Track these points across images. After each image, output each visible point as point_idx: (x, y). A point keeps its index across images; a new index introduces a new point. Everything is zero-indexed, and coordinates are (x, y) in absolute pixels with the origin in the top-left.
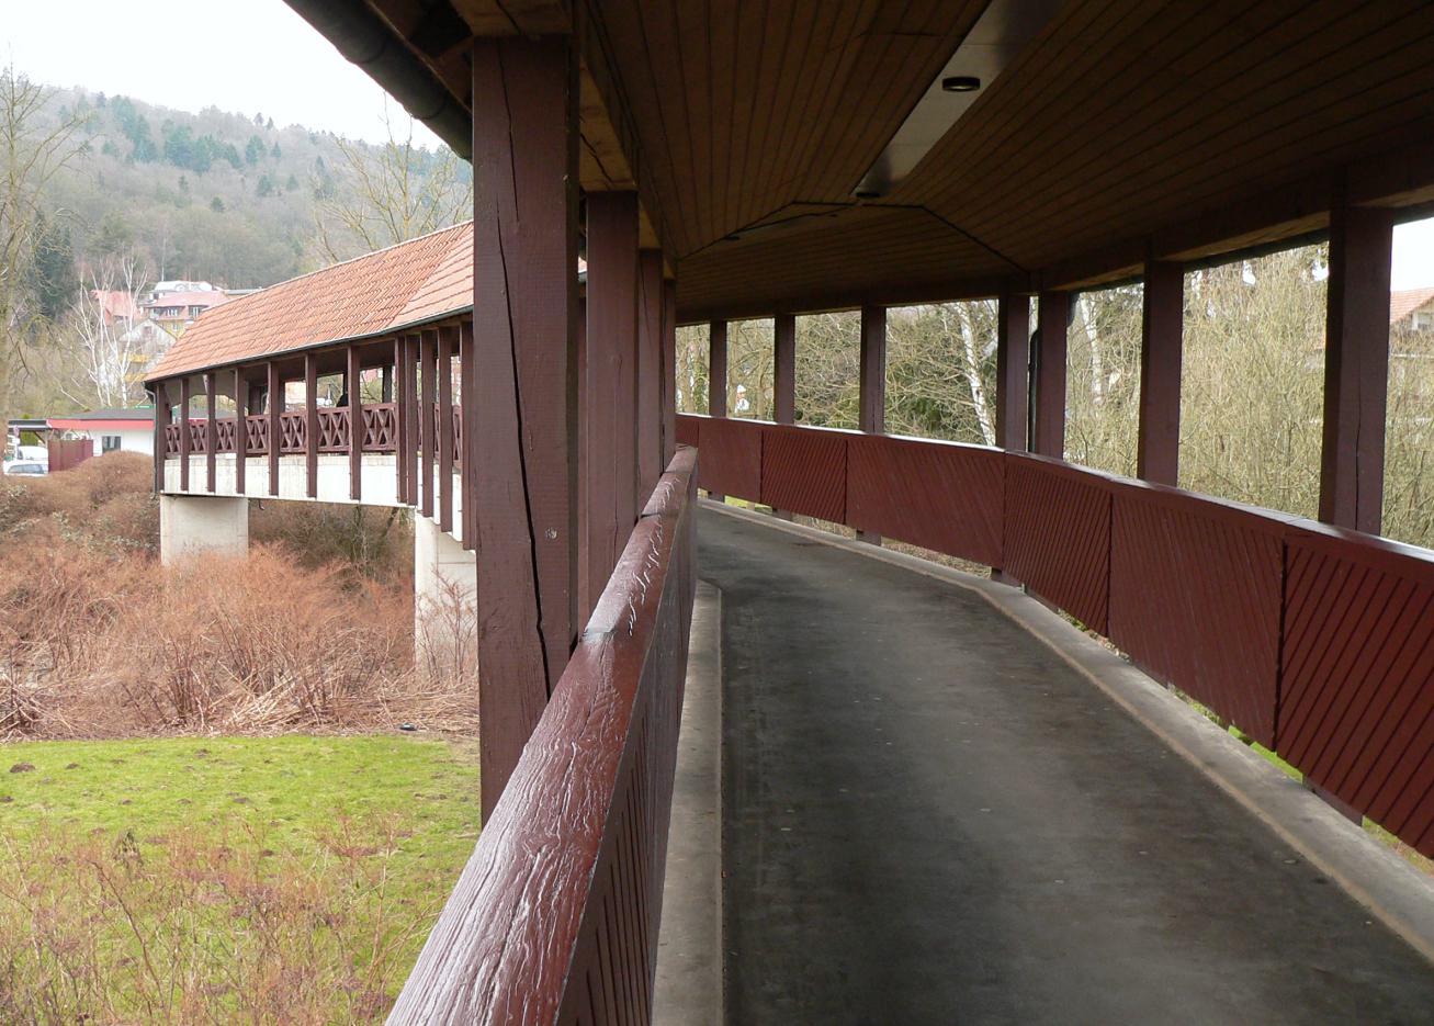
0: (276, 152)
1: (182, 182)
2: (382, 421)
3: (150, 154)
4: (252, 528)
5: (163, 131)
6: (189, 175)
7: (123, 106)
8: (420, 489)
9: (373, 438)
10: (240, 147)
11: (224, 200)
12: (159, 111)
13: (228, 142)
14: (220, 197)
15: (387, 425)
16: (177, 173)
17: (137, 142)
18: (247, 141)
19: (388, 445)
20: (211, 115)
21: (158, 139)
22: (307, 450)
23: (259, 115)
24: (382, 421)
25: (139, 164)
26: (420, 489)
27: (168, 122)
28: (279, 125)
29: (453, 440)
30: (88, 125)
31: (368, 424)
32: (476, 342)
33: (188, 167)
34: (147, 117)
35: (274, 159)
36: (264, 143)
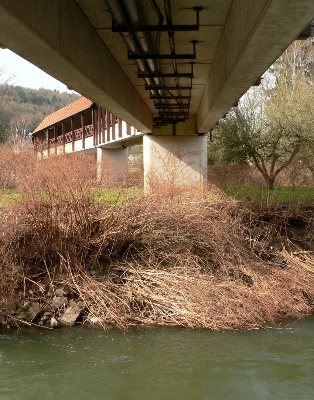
0: (60, 100)
1: (35, 108)
2: (90, 129)
3: (26, 101)
4: (75, 117)
5: (29, 95)
6: (36, 106)
7: (19, 89)
8: (98, 138)
9: (87, 134)
10: (50, 98)
11: (46, 112)
12: (28, 89)
13: (46, 97)
14: (45, 111)
15: (91, 130)
16: (33, 105)
17: (22, 98)
18: (52, 97)
19: (91, 134)
20: (42, 90)
21: (27, 96)
22: (72, 141)
23: (55, 90)
24: (90, 129)
25: (23, 103)
26: (98, 138)
27: (31, 92)
28: (61, 92)
29: (110, 119)
30: (10, 94)
31: (86, 131)
32: (127, 49)
33: (36, 104)
34: (25, 91)
35: (59, 101)
36: (57, 97)
